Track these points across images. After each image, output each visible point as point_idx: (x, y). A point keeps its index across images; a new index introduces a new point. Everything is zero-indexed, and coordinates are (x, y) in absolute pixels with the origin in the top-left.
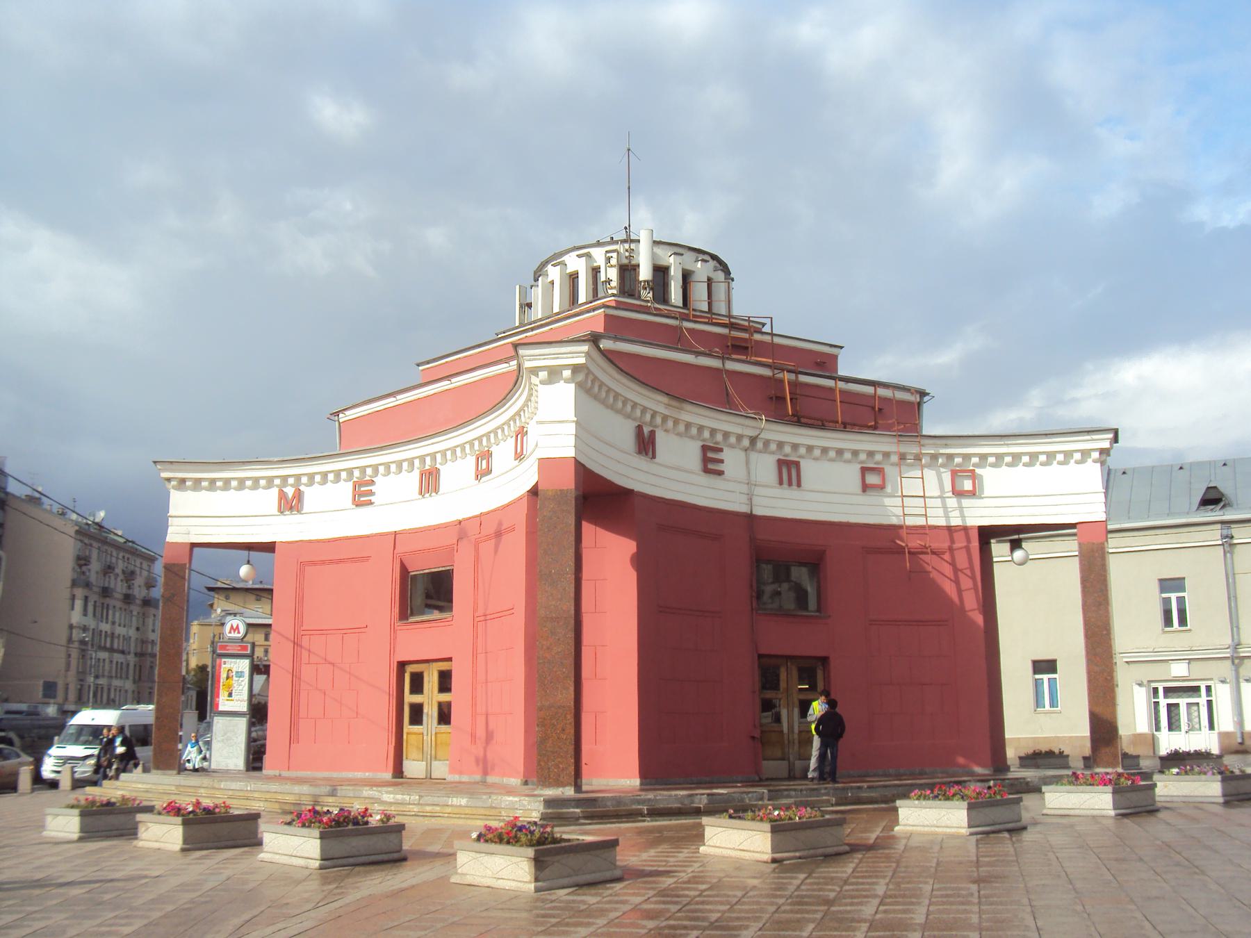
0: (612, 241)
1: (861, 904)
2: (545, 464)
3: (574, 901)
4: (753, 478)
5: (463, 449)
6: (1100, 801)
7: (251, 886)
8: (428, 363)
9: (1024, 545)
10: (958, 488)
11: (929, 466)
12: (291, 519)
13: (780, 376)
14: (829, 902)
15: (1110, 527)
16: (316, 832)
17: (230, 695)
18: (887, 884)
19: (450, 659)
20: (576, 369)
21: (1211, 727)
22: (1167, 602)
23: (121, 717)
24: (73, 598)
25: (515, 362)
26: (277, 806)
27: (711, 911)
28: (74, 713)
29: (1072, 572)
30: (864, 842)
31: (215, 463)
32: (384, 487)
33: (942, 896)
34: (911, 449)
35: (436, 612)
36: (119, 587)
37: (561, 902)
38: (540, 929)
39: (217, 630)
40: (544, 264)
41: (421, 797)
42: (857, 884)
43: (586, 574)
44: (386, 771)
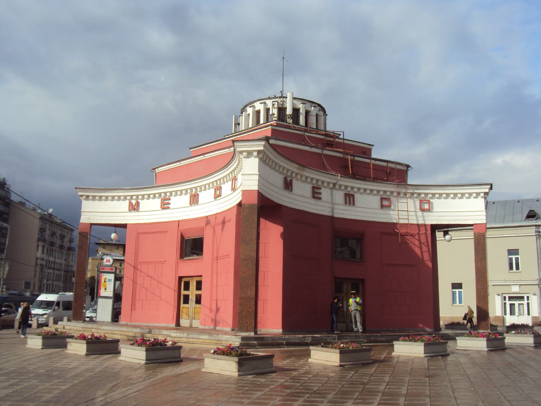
0: (275, 97)
1: (378, 385)
2: (244, 192)
3: (255, 381)
4: (334, 201)
5: (209, 186)
6: (479, 344)
7: (115, 371)
8: (195, 148)
9: (450, 233)
10: (422, 208)
11: (410, 198)
12: (134, 213)
13: (347, 157)
14: (364, 384)
15: (488, 226)
16: (144, 349)
17: (106, 289)
18: (390, 377)
19: (201, 276)
20: (259, 152)
21: (529, 314)
22: (511, 259)
23: (59, 297)
24: (38, 246)
25: (233, 148)
26: (126, 337)
27: (314, 386)
28: (38, 296)
29: (471, 245)
30: (380, 359)
31: (103, 189)
32: (175, 201)
33: (413, 382)
34: (403, 190)
35: (195, 256)
36: (58, 242)
37: (249, 381)
38: (241, 392)
39: (100, 261)
40: (246, 106)
41: (188, 335)
42: (377, 376)
43: (261, 241)
44: (173, 323)
